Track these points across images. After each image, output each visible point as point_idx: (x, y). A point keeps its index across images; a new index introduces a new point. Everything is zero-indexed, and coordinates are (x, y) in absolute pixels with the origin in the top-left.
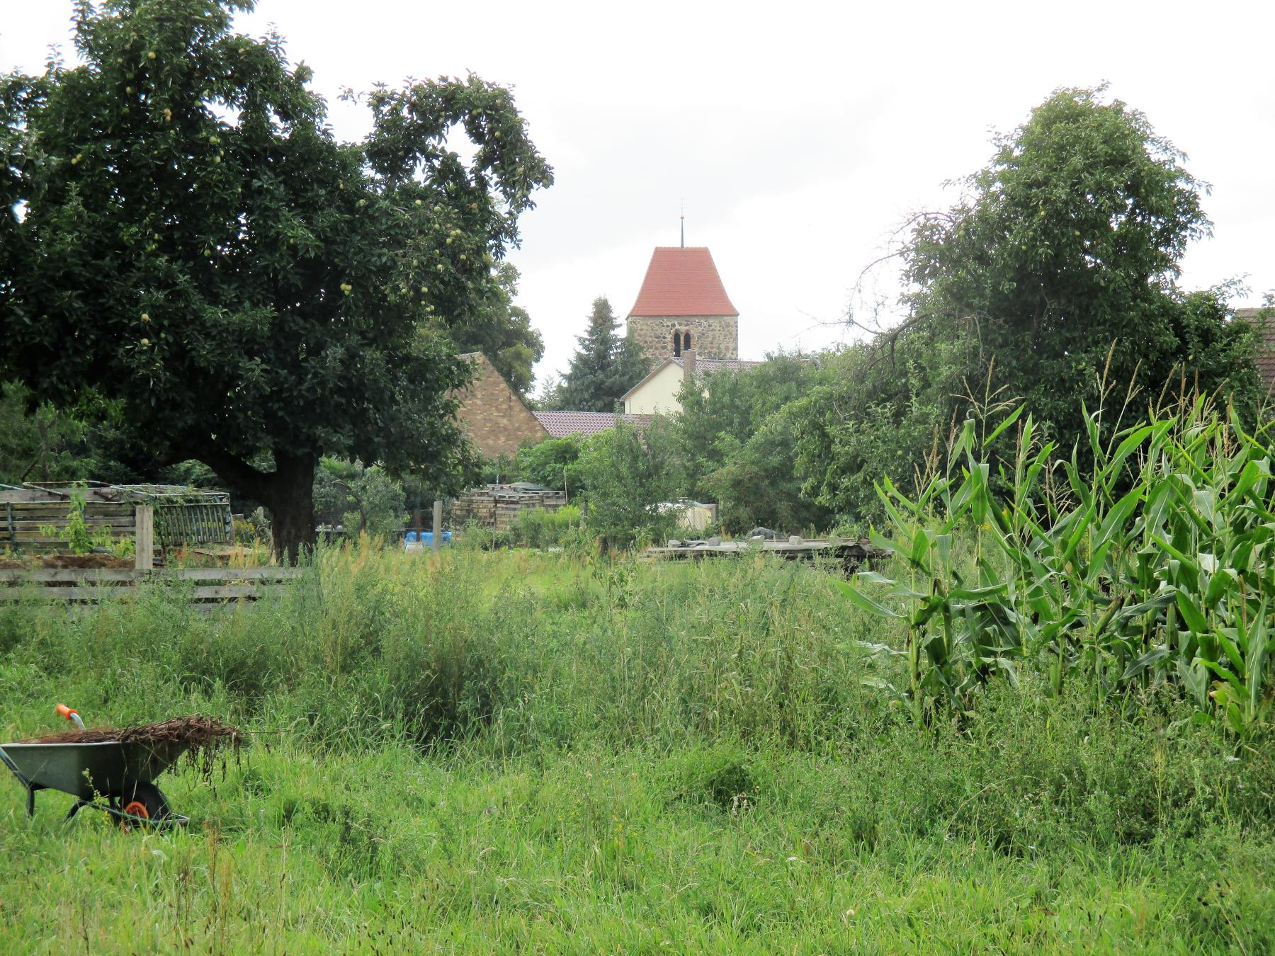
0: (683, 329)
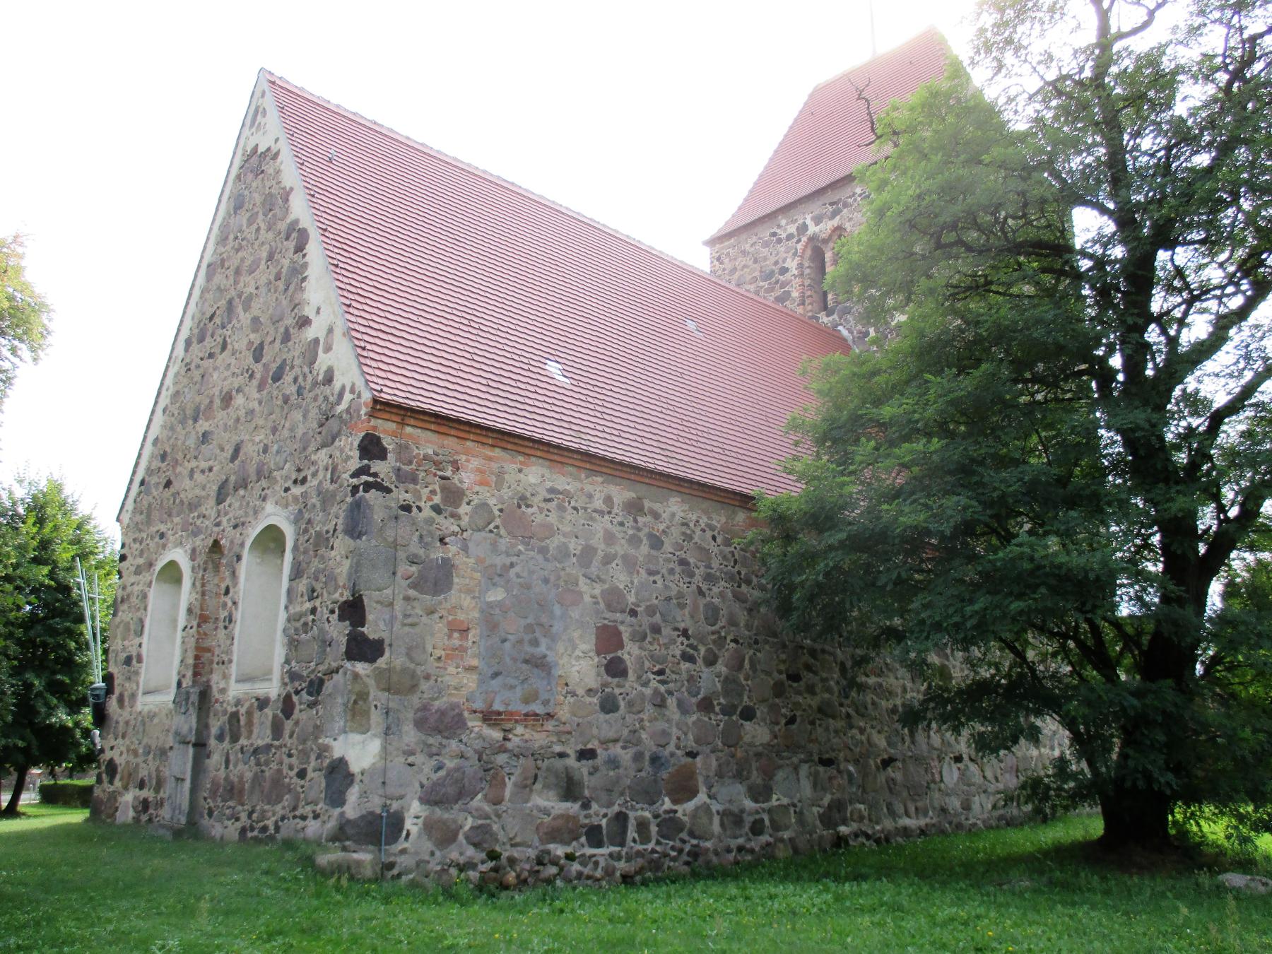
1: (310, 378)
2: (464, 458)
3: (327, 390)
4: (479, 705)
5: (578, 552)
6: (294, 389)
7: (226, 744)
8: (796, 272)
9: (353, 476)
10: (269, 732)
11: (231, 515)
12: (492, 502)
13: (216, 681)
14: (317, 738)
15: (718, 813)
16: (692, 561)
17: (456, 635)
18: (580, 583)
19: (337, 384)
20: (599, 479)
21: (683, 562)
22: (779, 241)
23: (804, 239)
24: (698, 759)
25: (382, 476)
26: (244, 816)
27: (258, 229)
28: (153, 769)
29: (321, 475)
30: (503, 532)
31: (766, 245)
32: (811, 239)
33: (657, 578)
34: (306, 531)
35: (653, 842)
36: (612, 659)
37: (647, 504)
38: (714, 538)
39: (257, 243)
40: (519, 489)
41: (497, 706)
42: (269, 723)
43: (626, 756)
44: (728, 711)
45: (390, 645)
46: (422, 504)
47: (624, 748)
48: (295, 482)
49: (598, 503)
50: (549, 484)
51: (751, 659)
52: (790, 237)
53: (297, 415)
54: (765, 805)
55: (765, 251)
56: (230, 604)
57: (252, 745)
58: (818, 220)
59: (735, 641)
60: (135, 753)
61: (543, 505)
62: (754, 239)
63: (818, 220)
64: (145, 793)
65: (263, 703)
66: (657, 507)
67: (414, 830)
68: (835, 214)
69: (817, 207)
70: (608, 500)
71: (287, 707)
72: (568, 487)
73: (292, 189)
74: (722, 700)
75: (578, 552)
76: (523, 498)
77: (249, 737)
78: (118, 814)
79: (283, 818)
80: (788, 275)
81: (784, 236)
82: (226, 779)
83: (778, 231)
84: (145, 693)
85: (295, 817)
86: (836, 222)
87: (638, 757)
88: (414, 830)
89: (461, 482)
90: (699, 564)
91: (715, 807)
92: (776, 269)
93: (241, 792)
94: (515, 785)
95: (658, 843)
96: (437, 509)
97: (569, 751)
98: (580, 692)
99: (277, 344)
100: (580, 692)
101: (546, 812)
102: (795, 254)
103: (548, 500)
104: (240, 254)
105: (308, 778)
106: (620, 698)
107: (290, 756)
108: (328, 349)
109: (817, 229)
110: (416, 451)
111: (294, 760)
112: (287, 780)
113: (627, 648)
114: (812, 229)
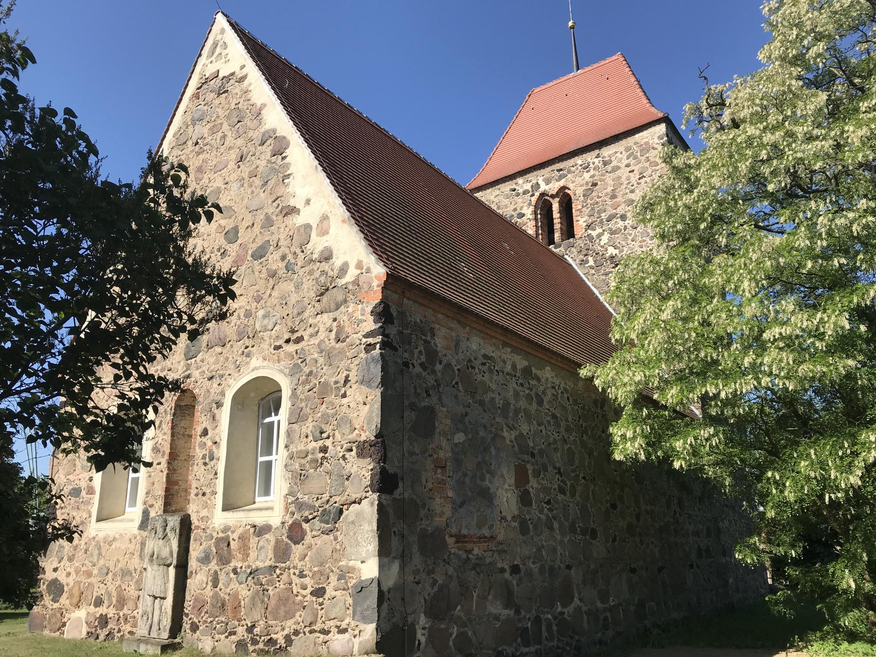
0: (553, 187)
1: (301, 256)
2: (437, 326)
3: (325, 266)
4: (454, 530)
5: (500, 406)
6: (282, 265)
7: (213, 566)
8: (531, 217)
9: (364, 336)
10: (271, 555)
11: (205, 368)
12: (454, 363)
13: (193, 509)
14: (337, 561)
15: (585, 612)
16: (558, 415)
17: (439, 471)
18: (504, 430)
19: (337, 262)
20: (509, 350)
21: (554, 416)
22: (518, 195)
23: (537, 194)
24: (573, 571)
25: (391, 337)
26: (241, 631)
27: (224, 137)
28: (112, 588)
29: (322, 335)
30: (461, 388)
31: (507, 197)
32: (543, 194)
33: (542, 428)
34: (307, 381)
35: (556, 639)
36: (524, 490)
37: (534, 370)
38: (568, 399)
39: (222, 149)
40: (468, 354)
41: (464, 532)
42: (270, 547)
43: (535, 568)
44: (584, 532)
45: (402, 479)
46: (414, 362)
47: (534, 563)
48: (288, 341)
49: (508, 368)
50: (483, 351)
51: (593, 491)
52: (526, 192)
53: (287, 287)
54: (607, 606)
55: (507, 201)
56: (209, 443)
57: (249, 566)
58: (548, 181)
59: (584, 478)
60: (89, 574)
61: (481, 367)
62: (498, 192)
63: (548, 181)
64: (102, 610)
65: (261, 531)
66: (539, 373)
67: (423, 640)
68: (560, 178)
69: (546, 172)
70: (514, 367)
71: (296, 533)
72: (493, 355)
73: (264, 106)
74: (581, 524)
75: (500, 406)
76: (470, 361)
77: (244, 560)
78: (66, 629)
79: (296, 633)
80: (524, 219)
81: (521, 191)
82: (216, 596)
83: (517, 188)
84: (99, 520)
85: (311, 632)
86: (562, 183)
87: (542, 570)
88: (423, 640)
89: (435, 345)
90: (562, 418)
91: (584, 609)
92: (515, 214)
93: (237, 608)
94: (478, 597)
95: (559, 640)
96: (422, 365)
97: (506, 567)
98: (509, 518)
99: (257, 229)
100: (509, 518)
101: (497, 618)
102: (530, 204)
103: (484, 364)
104: (201, 157)
105: (326, 596)
106: (529, 522)
107: (302, 575)
108: (324, 232)
109: (547, 188)
110: (410, 319)
111: (307, 581)
112: (300, 598)
113: (531, 484)
114: (543, 187)
